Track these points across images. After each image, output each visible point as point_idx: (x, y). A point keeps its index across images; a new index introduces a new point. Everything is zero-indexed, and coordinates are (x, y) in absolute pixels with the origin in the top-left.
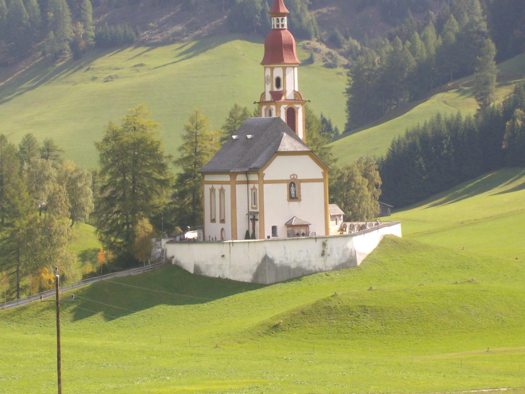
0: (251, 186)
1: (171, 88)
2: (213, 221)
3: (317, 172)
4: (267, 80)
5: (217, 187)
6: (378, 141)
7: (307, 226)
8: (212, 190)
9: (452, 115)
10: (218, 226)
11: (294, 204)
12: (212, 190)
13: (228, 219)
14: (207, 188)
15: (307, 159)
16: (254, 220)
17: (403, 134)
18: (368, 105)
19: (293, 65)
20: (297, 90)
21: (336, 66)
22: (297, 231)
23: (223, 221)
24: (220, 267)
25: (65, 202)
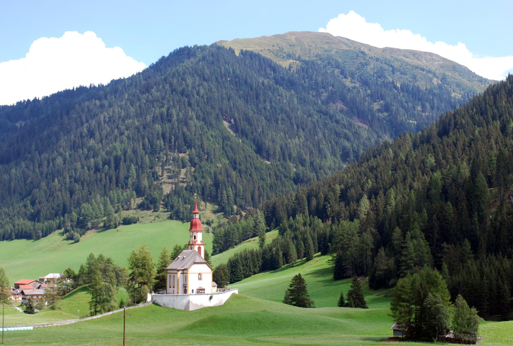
0: (185, 275)
1: (150, 235)
2: (170, 287)
3: (209, 270)
4: (191, 237)
5: (172, 275)
6: (224, 258)
7: (204, 290)
8: (170, 276)
9: (257, 250)
10: (172, 289)
11: (200, 281)
12: (170, 276)
13: (176, 287)
14: (168, 275)
15: (205, 266)
16: (185, 287)
17: (233, 255)
18: (222, 244)
19: (201, 231)
20: (111, 191)
21: (210, 226)
22: (201, 291)
23: (174, 287)
24: (173, 304)
25: (471, 264)
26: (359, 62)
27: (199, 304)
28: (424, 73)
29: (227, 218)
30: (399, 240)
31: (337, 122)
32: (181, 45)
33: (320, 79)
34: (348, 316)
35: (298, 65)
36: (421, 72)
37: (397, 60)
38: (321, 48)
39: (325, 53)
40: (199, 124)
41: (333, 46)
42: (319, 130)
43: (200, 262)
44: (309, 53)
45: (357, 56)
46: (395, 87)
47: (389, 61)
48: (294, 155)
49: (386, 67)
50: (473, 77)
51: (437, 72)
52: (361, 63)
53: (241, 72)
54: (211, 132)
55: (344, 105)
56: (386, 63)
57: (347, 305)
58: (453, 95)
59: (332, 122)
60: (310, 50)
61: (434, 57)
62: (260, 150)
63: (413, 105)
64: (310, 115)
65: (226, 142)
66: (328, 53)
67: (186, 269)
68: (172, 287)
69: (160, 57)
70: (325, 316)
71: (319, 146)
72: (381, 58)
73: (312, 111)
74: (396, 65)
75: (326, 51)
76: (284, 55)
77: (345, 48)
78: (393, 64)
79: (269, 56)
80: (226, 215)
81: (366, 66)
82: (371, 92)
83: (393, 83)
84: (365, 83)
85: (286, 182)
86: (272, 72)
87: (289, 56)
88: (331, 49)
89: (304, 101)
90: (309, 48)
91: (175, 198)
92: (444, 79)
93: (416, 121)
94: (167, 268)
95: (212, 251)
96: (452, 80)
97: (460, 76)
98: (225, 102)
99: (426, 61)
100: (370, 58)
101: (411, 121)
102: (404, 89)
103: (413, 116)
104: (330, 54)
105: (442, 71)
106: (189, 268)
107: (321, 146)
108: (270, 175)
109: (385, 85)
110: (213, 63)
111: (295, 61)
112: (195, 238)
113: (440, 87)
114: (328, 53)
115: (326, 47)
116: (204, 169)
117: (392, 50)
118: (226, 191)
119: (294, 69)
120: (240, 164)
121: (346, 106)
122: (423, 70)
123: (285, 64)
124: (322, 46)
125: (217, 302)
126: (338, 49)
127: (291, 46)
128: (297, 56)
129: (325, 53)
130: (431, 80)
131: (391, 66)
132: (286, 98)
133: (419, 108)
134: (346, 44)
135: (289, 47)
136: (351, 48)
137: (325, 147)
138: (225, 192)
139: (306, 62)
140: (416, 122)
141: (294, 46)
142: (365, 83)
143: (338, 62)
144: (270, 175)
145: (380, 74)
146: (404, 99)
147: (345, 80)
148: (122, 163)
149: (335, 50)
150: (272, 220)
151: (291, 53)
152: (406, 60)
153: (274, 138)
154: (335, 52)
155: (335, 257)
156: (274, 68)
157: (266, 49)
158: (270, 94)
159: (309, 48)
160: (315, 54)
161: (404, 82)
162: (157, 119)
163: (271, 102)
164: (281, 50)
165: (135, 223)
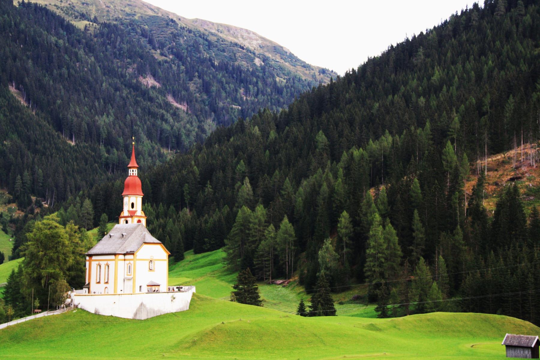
13: (111, 281)
26: (169, 32)
27: (156, 309)
28: (245, 51)
29: (23, 211)
30: (347, 228)
31: (151, 99)
33: (125, 46)
34: (372, 327)
35: (95, 28)
36: (241, 50)
37: (213, 34)
38: (122, 10)
39: (127, 18)
41: (137, 10)
42: (130, 107)
43: (152, 242)
44: (108, 15)
45: (168, 24)
46: (213, 65)
47: (204, 35)
48: (104, 136)
49: (201, 41)
50: (296, 61)
51: (257, 52)
52: (172, 33)
53: (27, 27)
55: (155, 80)
56: (200, 36)
57: (312, 314)
58: (278, 79)
59: (144, 100)
60: (108, 11)
61: (251, 35)
62: (59, 125)
63: (235, 87)
64: (117, 89)
66: (131, 17)
67: (132, 253)
68: (102, 281)
69: (450, 15)
71: (132, 127)
72: (193, 30)
73: (119, 85)
74: (212, 39)
75: (128, 15)
76: (77, 14)
77: (151, 13)
78: (209, 38)
79: (58, 12)
80: (21, 206)
81: (177, 37)
82: (186, 68)
83: (210, 60)
84: (178, 56)
86: (65, 33)
87: (83, 16)
88: (133, 13)
89: (109, 71)
90: (107, 9)
92: (265, 60)
93: (240, 106)
94: (92, 252)
95: (10, 254)
96: (273, 62)
97: (281, 58)
98: (10, 61)
99: (243, 38)
100: (181, 28)
101: (234, 106)
102: (224, 67)
103: (235, 100)
104: (133, 18)
105: (261, 51)
106: (138, 249)
107: (135, 127)
109: (202, 61)
111: (91, 23)
113: (263, 68)
114: (131, 17)
115: (127, 10)
117: (204, 22)
118: (22, 175)
119: (91, 30)
120: (36, 143)
121: (158, 82)
122: (243, 48)
123: (81, 24)
124: (122, 9)
125: (181, 306)
126: (142, 14)
127: (83, 4)
128: (92, 17)
129: (127, 18)
130: (252, 60)
131: (207, 40)
132: (87, 65)
133: (242, 91)
134: (152, 10)
135: (81, 6)
136: (158, 14)
139: (105, 25)
140: (240, 108)
141: (87, 4)
142: (178, 56)
143: (144, 30)
145: (195, 47)
146: (224, 80)
147: (153, 51)
149: (139, 15)
151: (85, 13)
152: (221, 35)
153: (77, 112)
154: (139, 17)
155: (231, 254)
156: (69, 29)
157: (53, 4)
158: (66, 57)
159: (107, 9)
160: (115, 17)
161: (223, 60)
163: (68, 69)
164: (72, 7)
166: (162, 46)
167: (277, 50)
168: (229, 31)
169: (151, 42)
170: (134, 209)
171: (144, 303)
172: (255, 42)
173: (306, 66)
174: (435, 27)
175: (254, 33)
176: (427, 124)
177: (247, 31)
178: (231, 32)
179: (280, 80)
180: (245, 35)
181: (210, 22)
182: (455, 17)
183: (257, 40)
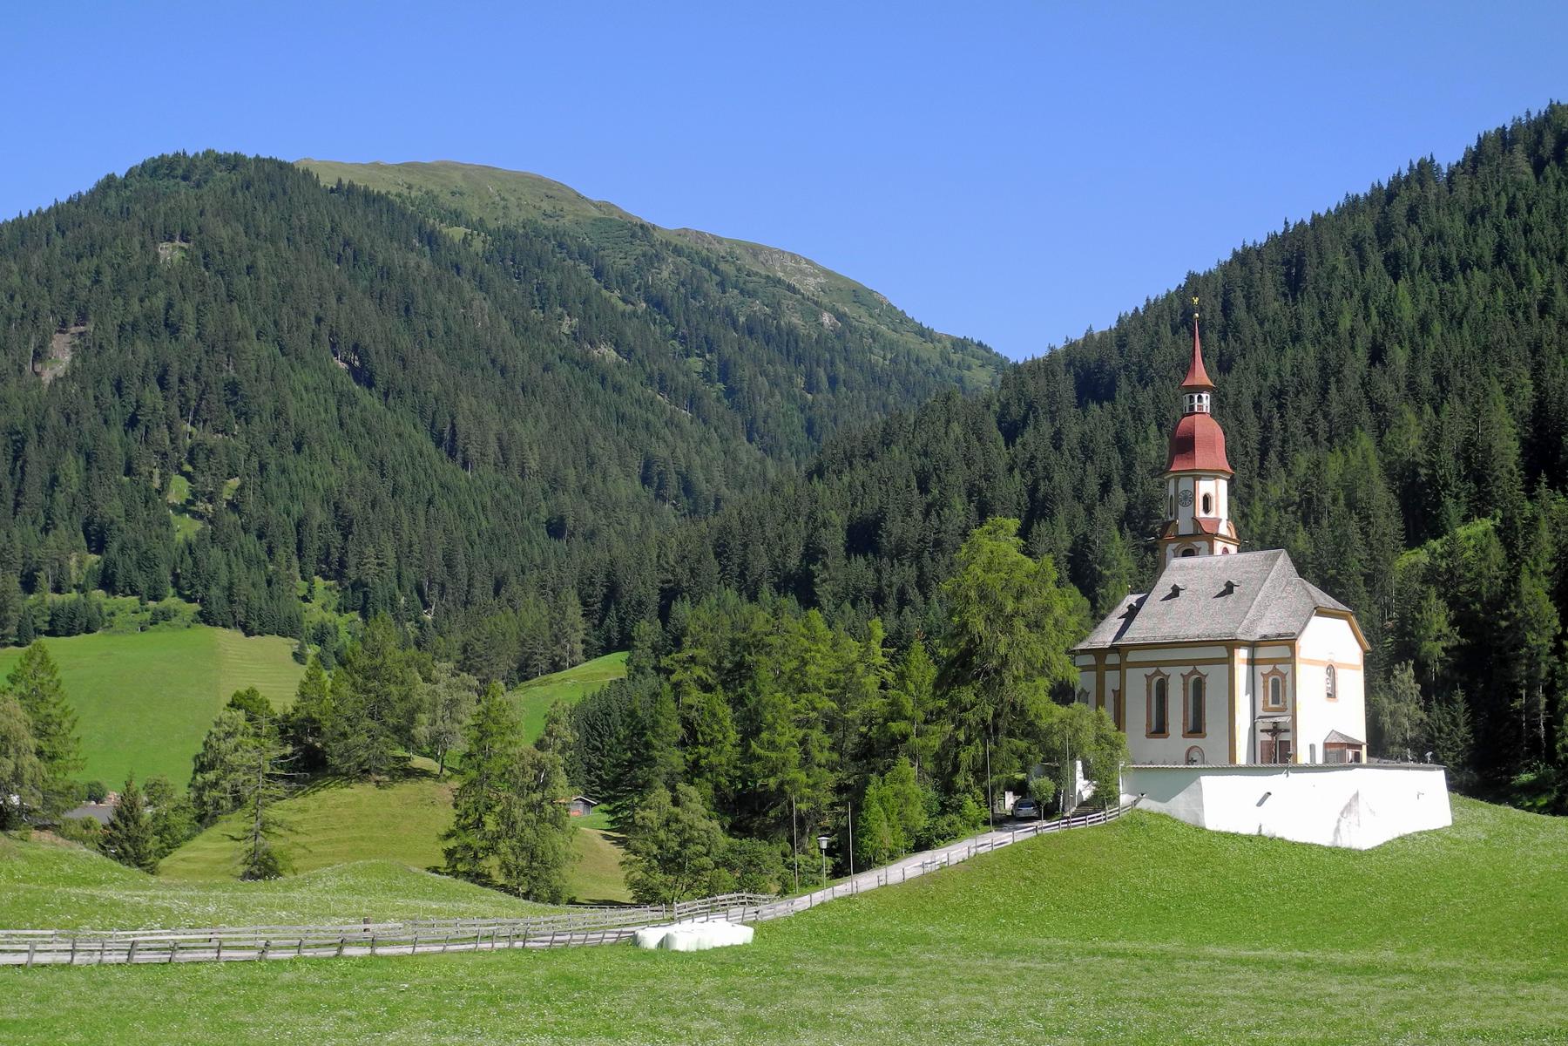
32: (167, 148)
40: (267, 350)
54: (307, 377)
61: (804, 265)
65: (346, 410)
69: (102, 177)
70: (135, 909)
77: (597, 214)
85: (1534, 270)
91: (216, 553)
108: (484, 508)
110: (272, 196)
112: (1207, 509)
115: (546, 206)
116: (294, 477)
117: (700, 236)
127: (453, 193)
130: (817, 317)
137: (601, 446)
138: (370, 551)
141: (461, 194)
144: (484, 508)
148: (31, 449)
150: (610, 618)
162: (134, 326)
165: (89, 630)
166: (624, 281)
167: (859, 295)
168: (755, 255)
169: (598, 274)
170: (1212, 515)
171: (229, 700)
172: (811, 281)
173: (924, 333)
174: (1235, 254)
175: (808, 262)
176: (1514, 448)
177: (793, 256)
178: (761, 258)
179: (878, 359)
180: (791, 264)
181: (714, 237)
182: (108, 184)
183: (815, 276)
